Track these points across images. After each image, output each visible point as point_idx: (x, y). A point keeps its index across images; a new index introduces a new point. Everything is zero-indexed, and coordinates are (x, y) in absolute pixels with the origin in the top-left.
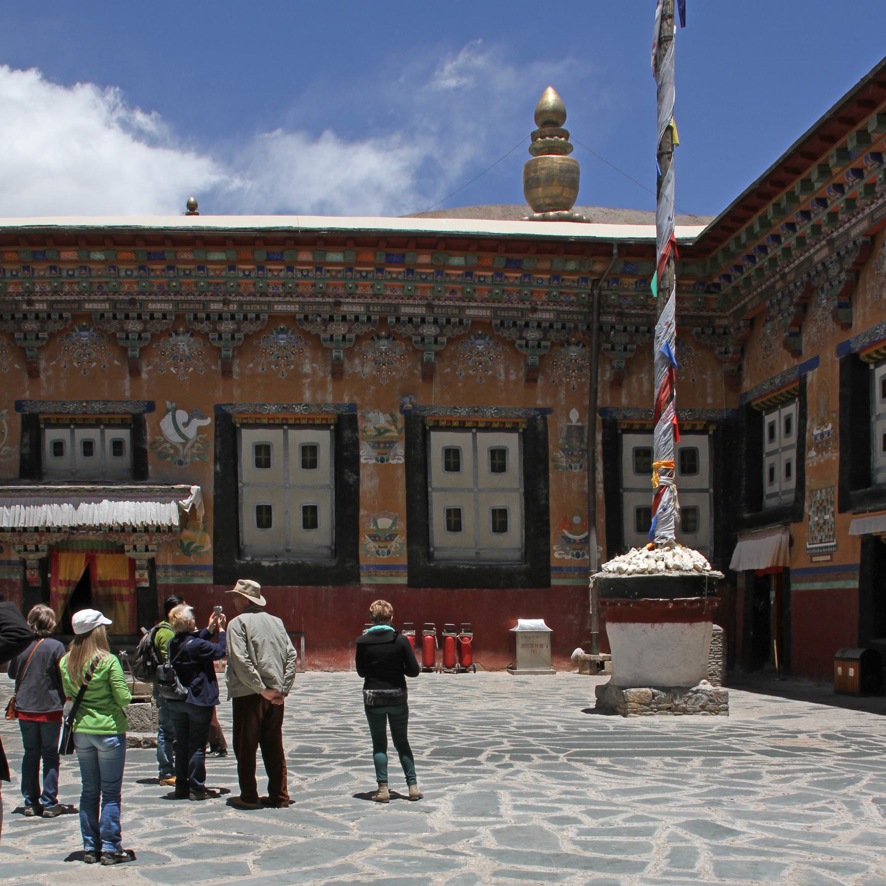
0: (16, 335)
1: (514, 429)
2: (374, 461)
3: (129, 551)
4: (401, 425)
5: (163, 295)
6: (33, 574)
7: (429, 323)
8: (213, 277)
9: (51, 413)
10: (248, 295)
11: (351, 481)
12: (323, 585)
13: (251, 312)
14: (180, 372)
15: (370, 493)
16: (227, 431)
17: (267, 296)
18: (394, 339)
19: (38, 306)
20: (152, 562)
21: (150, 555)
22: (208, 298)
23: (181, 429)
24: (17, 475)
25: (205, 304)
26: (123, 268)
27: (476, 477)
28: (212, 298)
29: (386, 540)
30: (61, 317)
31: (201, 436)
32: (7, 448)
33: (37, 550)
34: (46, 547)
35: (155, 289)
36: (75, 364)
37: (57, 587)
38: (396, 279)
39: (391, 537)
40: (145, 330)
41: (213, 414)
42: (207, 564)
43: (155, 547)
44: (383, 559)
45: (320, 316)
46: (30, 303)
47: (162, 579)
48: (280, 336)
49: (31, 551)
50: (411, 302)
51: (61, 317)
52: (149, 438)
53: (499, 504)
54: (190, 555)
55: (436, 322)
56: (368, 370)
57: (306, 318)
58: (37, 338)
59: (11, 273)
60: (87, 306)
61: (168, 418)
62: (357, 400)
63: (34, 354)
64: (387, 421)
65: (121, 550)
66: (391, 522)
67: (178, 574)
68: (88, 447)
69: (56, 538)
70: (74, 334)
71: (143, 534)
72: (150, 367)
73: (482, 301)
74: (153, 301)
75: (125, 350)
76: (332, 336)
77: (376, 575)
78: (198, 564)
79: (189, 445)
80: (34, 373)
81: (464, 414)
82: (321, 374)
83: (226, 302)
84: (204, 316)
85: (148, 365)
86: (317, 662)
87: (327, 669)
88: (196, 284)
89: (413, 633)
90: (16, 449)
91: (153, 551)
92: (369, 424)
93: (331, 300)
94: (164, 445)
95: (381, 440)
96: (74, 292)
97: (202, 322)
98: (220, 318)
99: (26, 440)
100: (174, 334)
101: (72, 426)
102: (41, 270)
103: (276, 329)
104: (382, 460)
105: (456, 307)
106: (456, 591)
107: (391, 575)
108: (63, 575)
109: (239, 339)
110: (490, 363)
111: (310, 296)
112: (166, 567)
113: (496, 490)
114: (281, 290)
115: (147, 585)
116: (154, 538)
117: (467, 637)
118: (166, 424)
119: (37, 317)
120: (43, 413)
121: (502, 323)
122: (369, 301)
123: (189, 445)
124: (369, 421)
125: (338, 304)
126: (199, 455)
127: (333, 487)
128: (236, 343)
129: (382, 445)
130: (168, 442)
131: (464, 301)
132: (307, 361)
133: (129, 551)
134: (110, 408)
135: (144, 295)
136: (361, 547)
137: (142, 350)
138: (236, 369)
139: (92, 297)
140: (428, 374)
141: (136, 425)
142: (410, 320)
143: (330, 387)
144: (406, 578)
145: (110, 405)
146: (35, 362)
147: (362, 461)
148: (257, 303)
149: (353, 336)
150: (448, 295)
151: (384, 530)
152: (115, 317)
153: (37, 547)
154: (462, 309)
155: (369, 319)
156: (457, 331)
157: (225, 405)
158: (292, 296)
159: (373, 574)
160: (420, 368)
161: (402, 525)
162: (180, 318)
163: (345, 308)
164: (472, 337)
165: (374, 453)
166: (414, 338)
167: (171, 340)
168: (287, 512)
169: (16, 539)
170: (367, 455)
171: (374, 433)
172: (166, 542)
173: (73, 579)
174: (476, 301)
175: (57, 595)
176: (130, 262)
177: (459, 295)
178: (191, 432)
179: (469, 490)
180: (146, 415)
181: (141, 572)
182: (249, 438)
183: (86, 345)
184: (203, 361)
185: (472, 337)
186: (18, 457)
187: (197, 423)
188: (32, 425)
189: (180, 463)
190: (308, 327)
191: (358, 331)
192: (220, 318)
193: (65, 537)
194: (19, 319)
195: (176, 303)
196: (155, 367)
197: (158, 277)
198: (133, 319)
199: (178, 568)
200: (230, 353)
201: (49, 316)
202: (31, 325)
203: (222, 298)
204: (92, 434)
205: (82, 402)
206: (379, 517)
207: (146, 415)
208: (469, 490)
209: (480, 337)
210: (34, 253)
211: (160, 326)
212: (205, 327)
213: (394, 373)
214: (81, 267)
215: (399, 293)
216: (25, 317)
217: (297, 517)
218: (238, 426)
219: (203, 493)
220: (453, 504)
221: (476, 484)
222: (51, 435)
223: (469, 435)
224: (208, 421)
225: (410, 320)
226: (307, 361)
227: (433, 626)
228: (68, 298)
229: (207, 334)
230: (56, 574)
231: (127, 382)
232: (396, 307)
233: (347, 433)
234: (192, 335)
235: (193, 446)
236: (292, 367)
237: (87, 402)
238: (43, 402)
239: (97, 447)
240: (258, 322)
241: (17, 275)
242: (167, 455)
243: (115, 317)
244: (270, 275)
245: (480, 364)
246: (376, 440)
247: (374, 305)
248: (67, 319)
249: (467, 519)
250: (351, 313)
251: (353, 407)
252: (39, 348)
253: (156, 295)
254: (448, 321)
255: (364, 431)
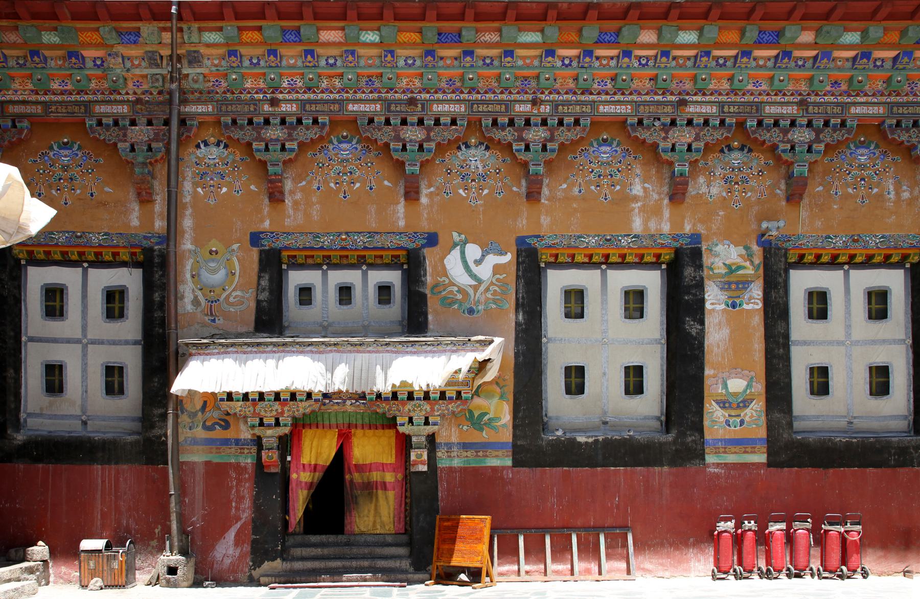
0: (255, 145)
1: (655, 265)
2: (723, 306)
3: (403, 425)
4: (758, 260)
5: (453, 92)
6: (271, 457)
7: (801, 126)
8: (520, 68)
9: (299, 249)
10: (566, 93)
11: (694, 332)
12: (655, 464)
13: (569, 115)
14: (472, 195)
15: (718, 347)
16: (530, 268)
17: (591, 94)
18: (750, 150)
19: (285, 108)
20: (431, 438)
21: (429, 429)
22: (513, 97)
23: (471, 268)
24: (251, 329)
25: (508, 105)
26: (401, 52)
27: (848, 327)
28: (518, 97)
29: (738, 406)
30: (315, 121)
31: (498, 276)
32: (238, 293)
33: (277, 423)
34: (289, 421)
35: (443, 84)
36: (332, 185)
37: (297, 473)
38: (764, 67)
39: (745, 403)
40: (428, 139)
41: (514, 249)
42: (504, 440)
43: (438, 419)
44: (735, 431)
45: (659, 119)
46: (274, 102)
47: (444, 461)
48: (603, 149)
49: (269, 426)
50: (778, 99)
51: (315, 121)
52: (429, 279)
53: (879, 359)
54: (481, 430)
55: (809, 124)
56: (716, 190)
57: (640, 122)
58: (283, 148)
59: (251, 60)
60: (350, 107)
61: (456, 252)
62: (701, 229)
63: (278, 169)
64: (741, 256)
65: (392, 423)
66: (745, 383)
67: (465, 454)
68: (345, 293)
69: (303, 407)
70: (331, 147)
71: (422, 402)
72: (432, 189)
73: (874, 95)
74: (439, 101)
75: (401, 165)
76: (674, 145)
77: (725, 452)
78: (492, 440)
79: (482, 288)
80: (276, 196)
81: (840, 244)
82: (656, 196)
83: (535, 102)
84: (507, 120)
85: (430, 186)
86: (648, 565)
87: (661, 574)
88: (499, 76)
89: (783, 526)
90: (250, 294)
91: (435, 424)
92: (717, 260)
93: (673, 98)
94: (450, 289)
95: (732, 279)
96: (334, 88)
97: (503, 129)
98: (528, 123)
99: (265, 283)
100: (463, 147)
101: (325, 267)
102: (291, 55)
103: (597, 140)
104: (734, 306)
105: (837, 104)
106: (831, 470)
107: (745, 452)
108: (307, 457)
109: (553, 151)
110: (876, 178)
111: (647, 94)
112: (449, 445)
113: (874, 342)
114: (609, 86)
115: (424, 468)
116: (436, 407)
117: (855, 532)
118: (453, 262)
119: (283, 122)
120: (287, 248)
121: (898, 124)
122: (724, 98)
123: (482, 288)
124: (717, 255)
125: (683, 103)
126: (495, 301)
127: (664, 341)
128: (549, 156)
129: (733, 286)
130: (454, 285)
131: (849, 95)
132: (637, 180)
133: (403, 425)
134: (378, 241)
135: (428, 92)
136: (706, 416)
137: (423, 165)
138: (545, 191)
139: (359, 96)
140: (794, 195)
141: (412, 265)
142: (776, 124)
143: (666, 213)
144: (765, 455)
145: (377, 237)
146: (280, 181)
147: (708, 306)
148: (578, 103)
149: (701, 145)
150: (828, 88)
151: (735, 394)
152: (388, 122)
153: (277, 420)
154: (845, 106)
155: (722, 122)
156: (838, 136)
157: (528, 237)
158: (623, 94)
159: (722, 450)
160: (783, 187)
161: (759, 387)
162: (474, 124)
163: (691, 109)
164: (852, 146)
165: (723, 296)
166: (782, 146)
167: (459, 154)
168: (604, 374)
169: (248, 409)
170: (714, 299)
171: (723, 271)
172: (453, 412)
173: (321, 462)
174: (866, 95)
175: (299, 482)
176: (414, 45)
177: (844, 87)
178: (485, 271)
179: (839, 343)
180: (426, 251)
181: (419, 451)
182: (557, 282)
183: (347, 160)
184: (501, 180)
185: (852, 146)
186: (253, 305)
187: (493, 260)
188: (273, 264)
189: (471, 311)
190: (642, 134)
191: (708, 139)
192: (528, 123)
193: (316, 407)
194: (259, 124)
195: (471, 104)
196: (438, 188)
197: (448, 67)
198: (412, 124)
199: (465, 446)
200: (541, 169)
201: (299, 121)
202: (275, 132)
203: (530, 97)
204: (351, 277)
205: (341, 234)
206: (729, 378)
207: (426, 251)
208: (839, 343)
209: (862, 145)
210: (284, 31)
211: (450, 134)
212: (507, 135)
213: (749, 194)
214: (346, 51)
215: (764, 87)
216: (267, 122)
217: (618, 381)
218: (543, 265)
219: (505, 346)
220: (818, 359)
221: (848, 335)
222: (296, 278)
223: (840, 273)
224: (508, 258)
225: (776, 124)
226: (637, 180)
227: (808, 517)
228: (325, 96)
229: (115, 144)
230: (299, 457)
231: (401, 208)
232: (759, 106)
233: (689, 271)
234: (487, 148)
235: (487, 290)
236: (618, 187)
237: (347, 233)
238: (288, 234)
239: (357, 293)
240: (578, 128)
241: (258, 63)
242: (454, 302)
243: (388, 122)
244: (597, 64)
245: (863, 179)
246: (726, 279)
247: (730, 104)
248: (324, 124)
249: (836, 380)
250: (699, 115)
251: (696, 238)
252: (285, 162)
253: (444, 92)
254: (826, 124)
255: (712, 269)
